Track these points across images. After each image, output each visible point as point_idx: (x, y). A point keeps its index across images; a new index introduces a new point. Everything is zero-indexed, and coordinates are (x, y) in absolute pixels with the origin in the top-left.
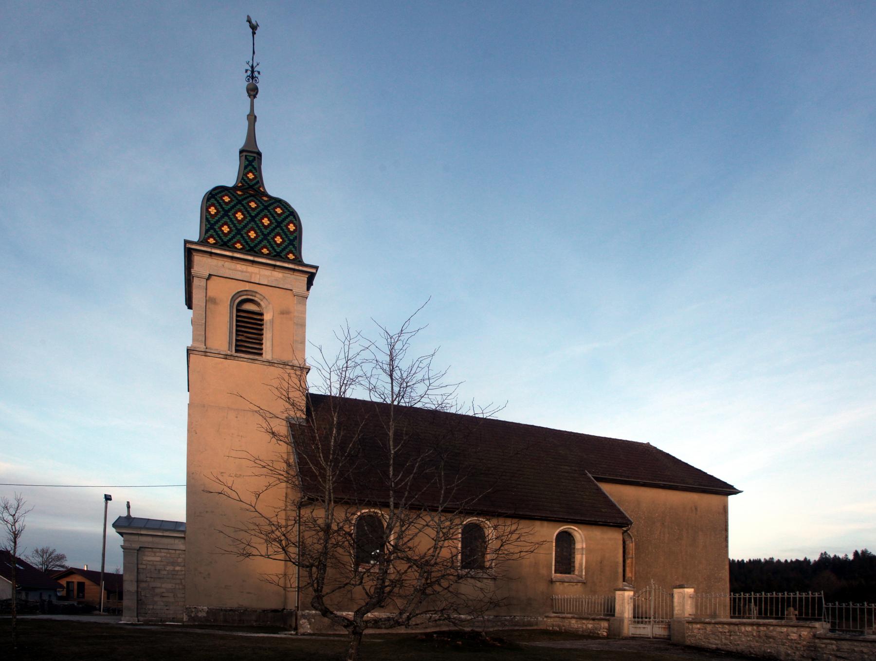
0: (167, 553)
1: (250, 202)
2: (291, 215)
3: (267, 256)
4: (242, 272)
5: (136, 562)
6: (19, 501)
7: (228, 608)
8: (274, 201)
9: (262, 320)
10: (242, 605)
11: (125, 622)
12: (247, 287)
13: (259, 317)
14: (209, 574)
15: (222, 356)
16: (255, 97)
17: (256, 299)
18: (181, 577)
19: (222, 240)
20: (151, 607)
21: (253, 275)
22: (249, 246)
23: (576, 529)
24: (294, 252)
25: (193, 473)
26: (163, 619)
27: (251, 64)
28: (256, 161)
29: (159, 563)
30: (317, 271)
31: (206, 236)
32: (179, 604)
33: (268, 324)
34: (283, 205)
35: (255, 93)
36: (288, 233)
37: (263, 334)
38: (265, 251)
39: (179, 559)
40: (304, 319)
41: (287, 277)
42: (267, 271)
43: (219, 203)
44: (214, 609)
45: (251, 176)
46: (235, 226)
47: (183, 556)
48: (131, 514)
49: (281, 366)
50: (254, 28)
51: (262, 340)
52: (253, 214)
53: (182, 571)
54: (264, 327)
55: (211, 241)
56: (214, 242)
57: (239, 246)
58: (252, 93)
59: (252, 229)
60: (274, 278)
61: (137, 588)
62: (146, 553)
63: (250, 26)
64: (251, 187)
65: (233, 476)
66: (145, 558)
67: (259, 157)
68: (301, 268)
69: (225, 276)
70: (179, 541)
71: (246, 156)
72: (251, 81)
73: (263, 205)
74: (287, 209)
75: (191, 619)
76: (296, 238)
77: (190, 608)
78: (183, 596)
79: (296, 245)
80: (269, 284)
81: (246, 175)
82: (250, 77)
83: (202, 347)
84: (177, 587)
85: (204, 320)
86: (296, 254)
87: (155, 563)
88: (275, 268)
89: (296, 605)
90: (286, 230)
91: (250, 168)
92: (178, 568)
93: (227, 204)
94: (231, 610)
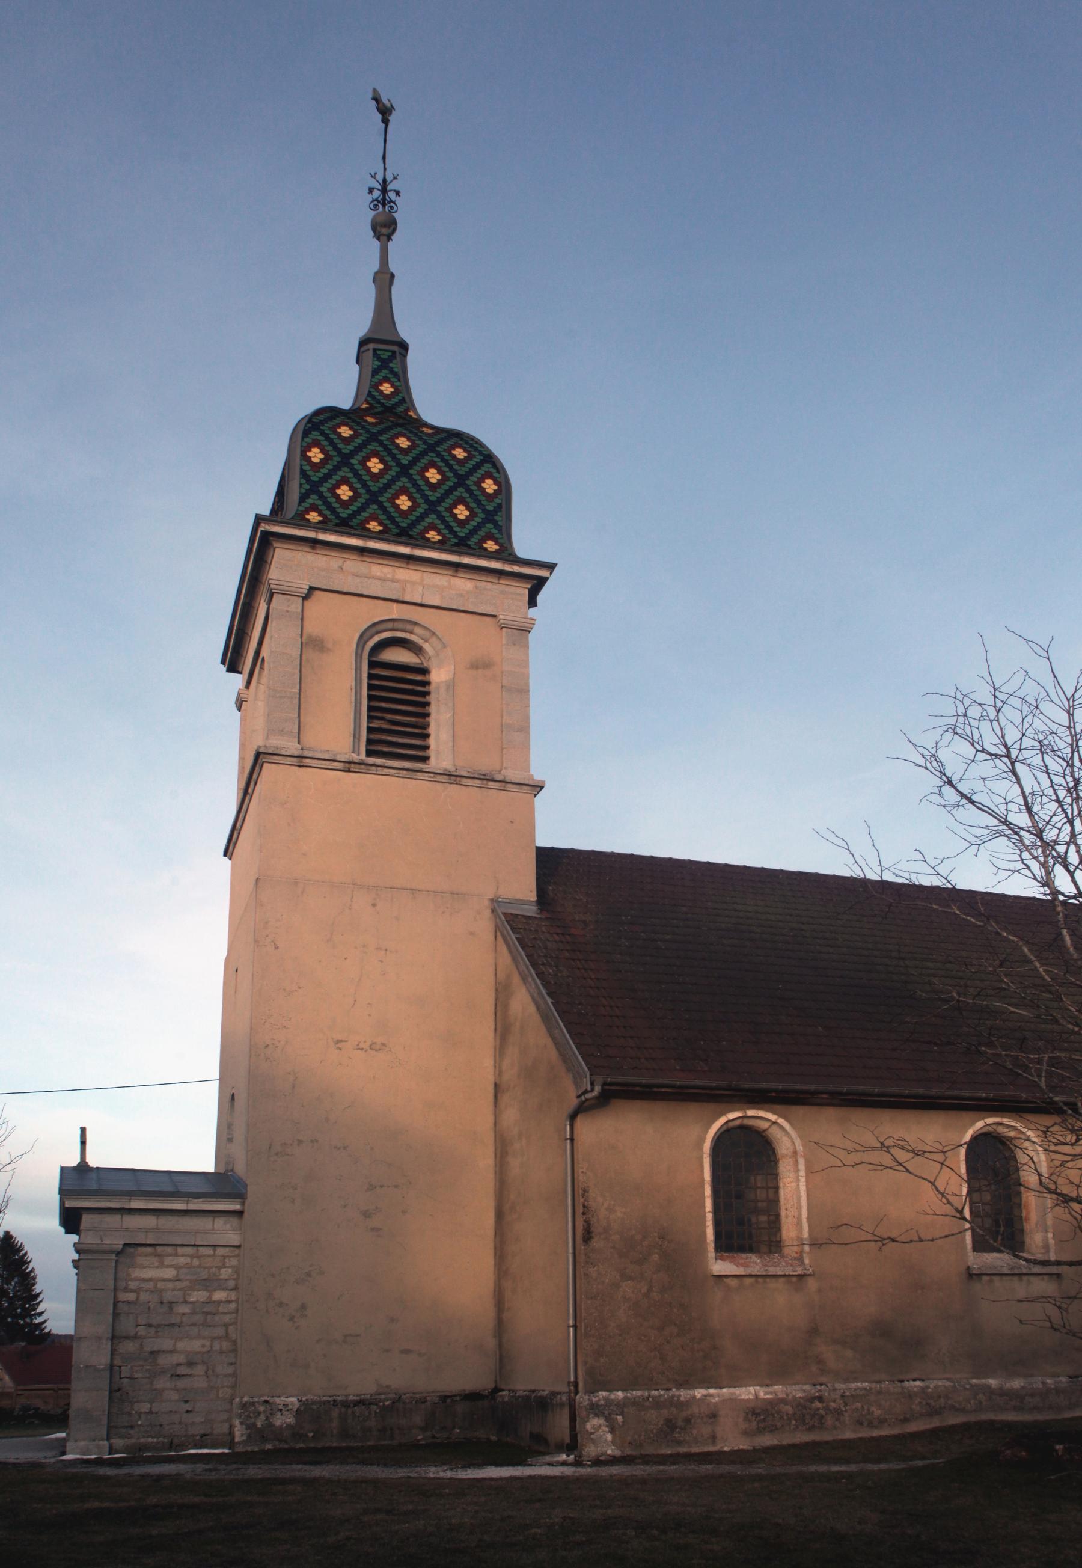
0: (192, 1257)
1: (397, 436)
2: (487, 462)
3: (440, 546)
4: (384, 580)
5: (112, 1287)
7: (351, 1398)
9: (427, 683)
10: (388, 1387)
11: (78, 1456)
12: (395, 612)
13: (419, 678)
14: (303, 1307)
15: (340, 766)
16: (389, 238)
17: (413, 638)
18: (227, 1319)
19: (338, 516)
20: (145, 1407)
21: (408, 585)
23: (773, 1117)
25: (267, 1046)
26: (176, 1441)
27: (380, 177)
29: (170, 1285)
31: (301, 508)
32: (221, 1396)
33: (442, 690)
34: (467, 443)
35: (390, 231)
36: (482, 498)
37: (428, 715)
38: (433, 535)
39: (223, 1271)
40: (527, 677)
41: (485, 589)
44: (314, 1403)
45: (387, 388)
46: (365, 485)
47: (234, 1262)
48: (87, 1160)
49: (478, 783)
50: (385, 112)
51: (426, 726)
52: (405, 461)
53: (230, 1302)
54: (432, 698)
55: (314, 517)
56: (321, 519)
57: (374, 526)
58: (384, 231)
59: (404, 491)
61: (112, 1359)
62: (140, 1260)
63: (378, 109)
64: (390, 410)
65: (366, 1046)
66: (137, 1273)
67: (403, 352)
68: (516, 569)
70: (225, 1223)
71: (375, 350)
72: (381, 209)
73: (425, 442)
74: (476, 449)
75: (256, 1434)
76: (499, 506)
77: (253, 1404)
78: (230, 1370)
79: (500, 523)
80: (444, 606)
81: (376, 386)
82: (379, 202)
83: (292, 747)
84: (217, 1346)
85: (298, 686)
86: (500, 541)
87: (160, 1285)
88: (456, 571)
89: (572, 1379)
90: (477, 493)
91: (384, 373)
92: (219, 1295)
93: (347, 441)
94: (357, 1403)
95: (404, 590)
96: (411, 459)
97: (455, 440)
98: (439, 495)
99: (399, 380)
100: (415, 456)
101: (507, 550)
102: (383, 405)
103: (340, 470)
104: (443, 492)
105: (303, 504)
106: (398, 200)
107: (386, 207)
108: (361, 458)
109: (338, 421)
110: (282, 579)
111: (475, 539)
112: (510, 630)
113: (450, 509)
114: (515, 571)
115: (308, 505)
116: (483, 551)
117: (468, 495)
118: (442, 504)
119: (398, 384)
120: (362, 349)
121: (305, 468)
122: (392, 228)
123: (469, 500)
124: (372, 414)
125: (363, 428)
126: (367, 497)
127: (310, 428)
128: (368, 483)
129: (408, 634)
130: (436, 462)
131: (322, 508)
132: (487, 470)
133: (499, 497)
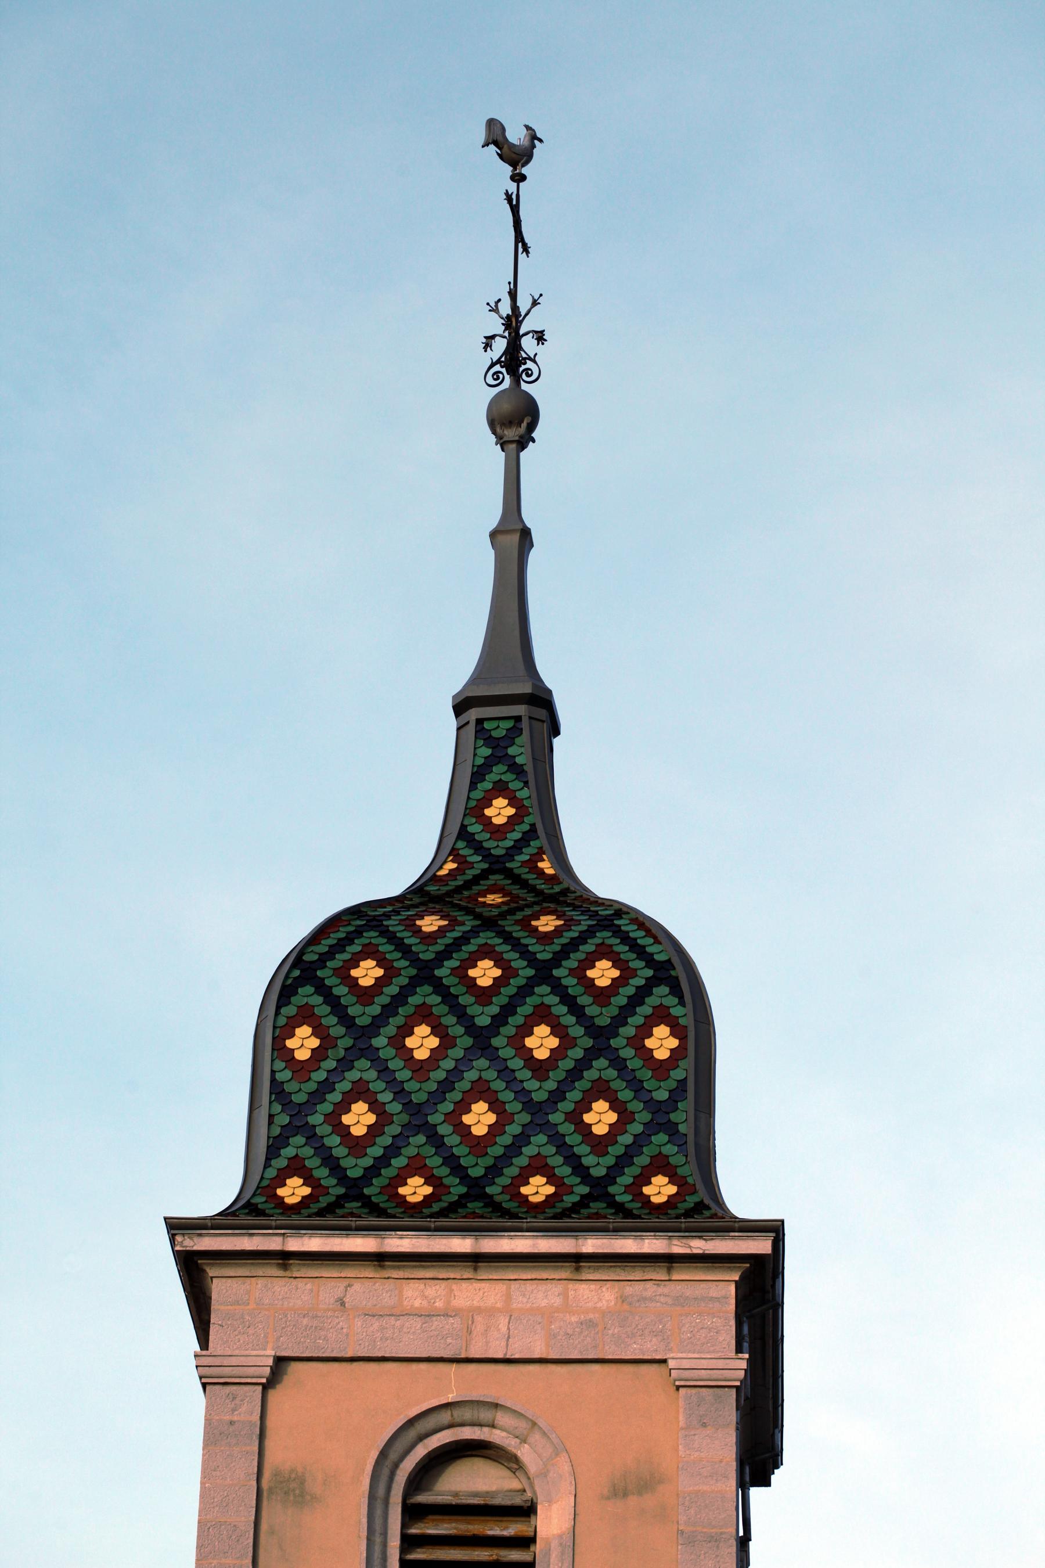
4: (427, 1315)
6: (486, 351)
13: (512, 1529)
16: (524, 442)
21: (478, 1319)
24: (677, 1160)
27: (505, 309)
28: (524, 739)
42: (543, 1287)
46: (400, 1093)
58: (511, 433)
60: (574, 1319)
63: (501, 156)
67: (542, 713)
81: (477, 810)
88: (578, 1269)
95: (470, 1332)
112: (694, 1391)
114: (695, 1251)
121: (279, 1077)
122: (524, 425)
127: (295, 978)
129: (486, 1429)
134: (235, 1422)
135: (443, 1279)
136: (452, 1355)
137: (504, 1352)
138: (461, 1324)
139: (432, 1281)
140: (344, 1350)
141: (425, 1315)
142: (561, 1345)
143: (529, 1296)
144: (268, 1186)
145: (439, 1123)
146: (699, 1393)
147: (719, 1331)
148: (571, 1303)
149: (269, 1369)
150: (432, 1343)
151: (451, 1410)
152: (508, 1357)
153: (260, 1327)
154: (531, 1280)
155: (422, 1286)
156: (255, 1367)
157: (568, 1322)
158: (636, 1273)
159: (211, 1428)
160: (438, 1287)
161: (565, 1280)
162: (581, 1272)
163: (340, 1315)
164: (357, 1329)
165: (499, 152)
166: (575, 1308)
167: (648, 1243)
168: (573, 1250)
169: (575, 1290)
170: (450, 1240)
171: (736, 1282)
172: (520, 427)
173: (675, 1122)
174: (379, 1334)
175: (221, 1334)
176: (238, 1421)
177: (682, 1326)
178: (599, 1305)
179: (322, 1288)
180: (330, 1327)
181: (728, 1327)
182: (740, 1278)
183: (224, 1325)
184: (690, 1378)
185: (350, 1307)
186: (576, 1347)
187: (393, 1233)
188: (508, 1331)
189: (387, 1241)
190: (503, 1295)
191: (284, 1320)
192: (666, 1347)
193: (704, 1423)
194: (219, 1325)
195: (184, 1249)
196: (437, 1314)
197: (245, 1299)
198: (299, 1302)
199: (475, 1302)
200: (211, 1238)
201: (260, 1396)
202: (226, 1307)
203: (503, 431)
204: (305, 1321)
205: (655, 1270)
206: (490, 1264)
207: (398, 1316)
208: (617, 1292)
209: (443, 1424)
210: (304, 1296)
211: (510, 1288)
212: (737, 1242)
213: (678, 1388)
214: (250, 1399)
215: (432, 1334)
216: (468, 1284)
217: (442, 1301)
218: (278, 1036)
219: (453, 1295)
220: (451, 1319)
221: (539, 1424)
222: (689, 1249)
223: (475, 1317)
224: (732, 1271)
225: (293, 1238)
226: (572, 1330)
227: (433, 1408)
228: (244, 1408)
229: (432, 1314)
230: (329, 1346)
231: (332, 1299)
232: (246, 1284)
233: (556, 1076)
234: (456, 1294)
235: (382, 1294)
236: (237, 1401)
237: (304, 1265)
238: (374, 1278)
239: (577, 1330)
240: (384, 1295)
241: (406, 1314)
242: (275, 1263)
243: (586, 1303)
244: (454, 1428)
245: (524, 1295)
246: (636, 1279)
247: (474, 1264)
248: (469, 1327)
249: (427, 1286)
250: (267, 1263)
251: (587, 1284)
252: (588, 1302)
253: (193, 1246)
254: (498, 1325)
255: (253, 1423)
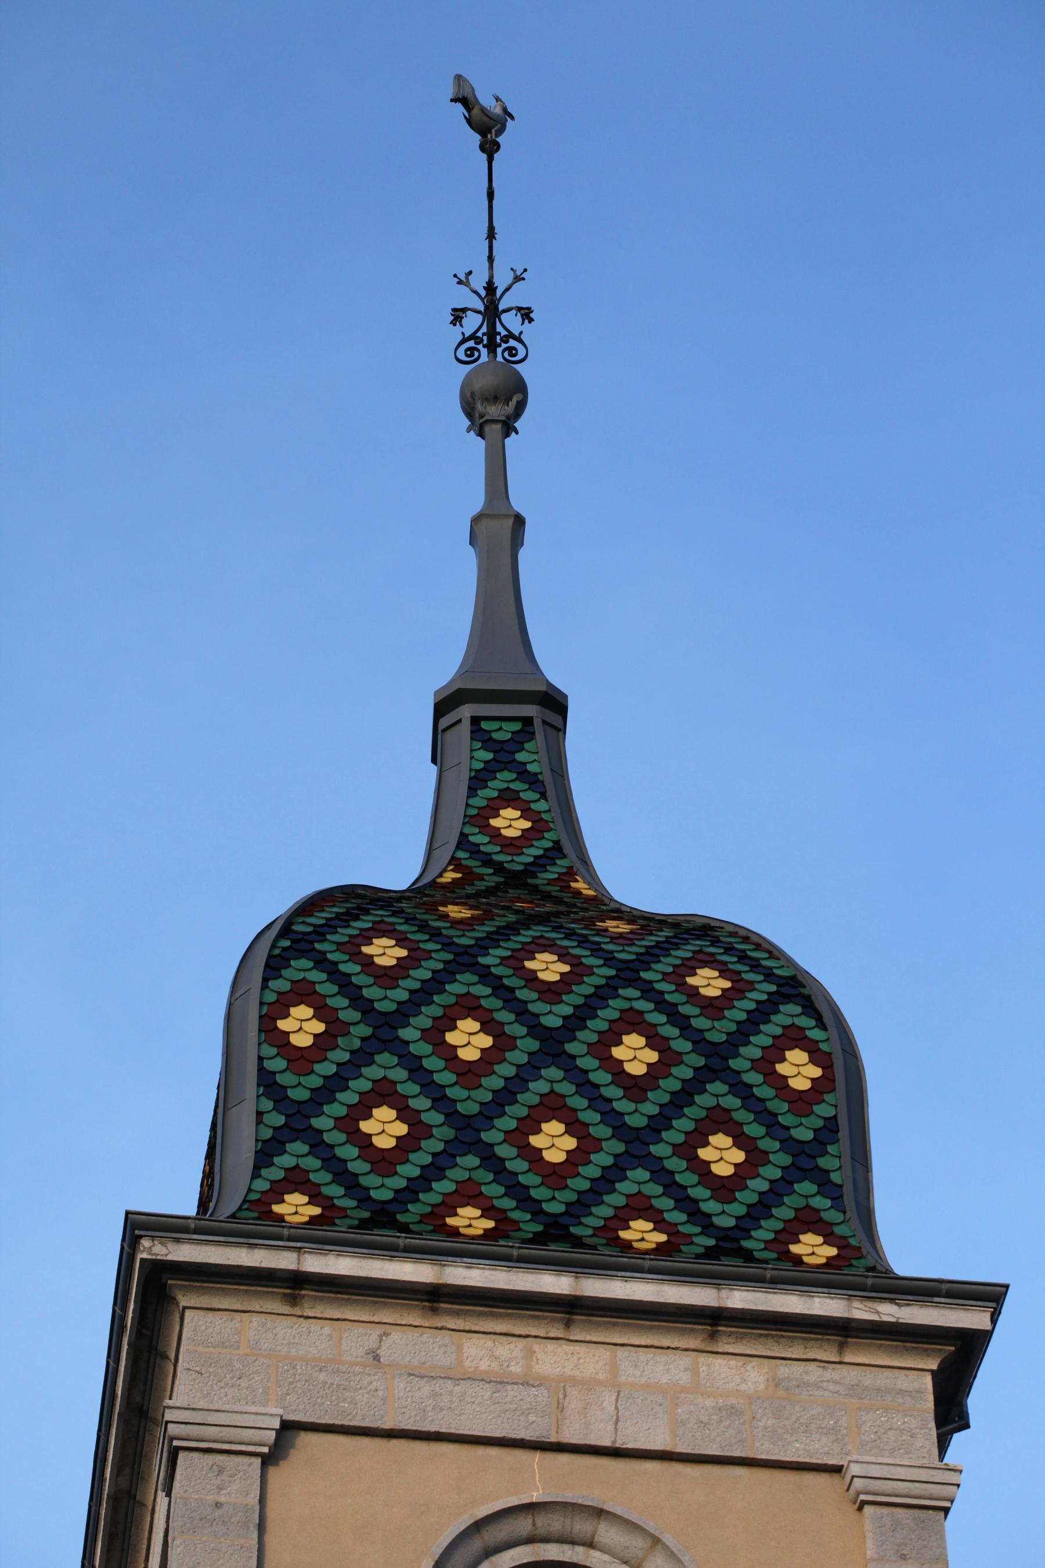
1: (689, 967)
2: (788, 999)
4: (500, 1382)
8: (667, 933)
16: (508, 428)
19: (364, 1198)
21: (572, 1392)
22: (537, 1212)
27: (479, 282)
30: (994, 1320)
31: (261, 1185)
34: (729, 950)
41: (803, 1385)
42: (662, 1357)
43: (345, 985)
46: (440, 1100)
58: (494, 411)
60: (709, 1403)
63: (469, 121)
67: (554, 719)
68: (888, 1312)
69: (388, 1424)
71: (475, 721)
73: (609, 960)
74: (755, 966)
76: (831, 1126)
79: (836, 1177)
80: (682, 1448)
81: (481, 819)
82: (479, 341)
86: (839, 1230)
88: (713, 1336)
90: (764, 1092)
91: (504, 779)
93: (387, 977)
96: (569, 1010)
97: (696, 944)
98: (655, 1110)
99: (544, 796)
100: (581, 1001)
101: (861, 1257)
102: (499, 868)
103: (371, 1063)
104: (666, 1098)
105: (264, 1172)
106: (528, 331)
107: (499, 350)
108: (428, 1023)
109: (364, 923)
110: (202, 1404)
111: (764, 1233)
112: (886, 1510)
113: (688, 1149)
114: (885, 1318)
115: (280, 1175)
116: (788, 1265)
117: (737, 1102)
118: (665, 1135)
119: (542, 806)
120: (444, 722)
121: (270, 1065)
122: (513, 403)
123: (741, 1116)
124: (469, 896)
125: (435, 935)
126: (449, 1133)
127: (284, 949)
128: (449, 1092)
129: (580, 1549)
130: (641, 1013)
131: (321, 1177)
132: (788, 1021)
133: (829, 1098)
134: (221, 1504)
135: (520, 1336)
136: (537, 1437)
137: (612, 1439)
138: (549, 1397)
139: (505, 1338)
140: (380, 1419)
141: (496, 1382)
142: (693, 1436)
143: (644, 1368)
144: (259, 1200)
145: (497, 1142)
146: (893, 1513)
147: (914, 1434)
148: (702, 1382)
149: (273, 1434)
150: (508, 1419)
151: (533, 1515)
152: (617, 1445)
153: (257, 1378)
154: (646, 1347)
155: (490, 1344)
156: (253, 1430)
157: (701, 1406)
158: (794, 1348)
159: (187, 1509)
160: (512, 1346)
161: (694, 1350)
162: (717, 1341)
163: (372, 1373)
164: (399, 1392)
165: (467, 114)
166: (709, 1389)
167: (820, 1302)
168: (714, 1303)
169: (708, 1365)
170: (539, 1276)
171: (932, 1371)
172: (508, 405)
173: (825, 1168)
174: (430, 1401)
175: (200, 1385)
176: (227, 1503)
177: (862, 1424)
178: (743, 1387)
179: (346, 1335)
180: (359, 1386)
181: (927, 1431)
182: (938, 1367)
183: (203, 1373)
184: (880, 1492)
185: (387, 1363)
186: (714, 1440)
187: (458, 1260)
188: (616, 1412)
189: (448, 1270)
190: (606, 1364)
191: (291, 1372)
192: (842, 1449)
193: (903, 1554)
194: (196, 1371)
195: (154, 1257)
196: (513, 1381)
197: (234, 1340)
198: (313, 1351)
199: (566, 1370)
200: (193, 1247)
201: (259, 1471)
202: (207, 1350)
203: (485, 409)
204: (322, 1377)
205: (821, 1346)
206: (590, 1318)
207: (458, 1380)
208: (767, 1373)
209: (521, 1536)
210: (321, 1343)
211: (616, 1356)
212: (942, 1311)
213: (864, 1503)
214: (245, 1474)
215: (506, 1407)
216: (556, 1346)
217: (520, 1364)
218: (266, 1014)
219: (534, 1358)
220: (534, 1389)
221: (665, 1540)
222: (877, 1315)
223: (568, 1390)
224: (928, 1355)
225: (313, 1256)
226: (707, 1418)
227: (510, 1508)
228: (235, 1487)
229: (505, 1380)
230: (359, 1412)
231: (361, 1350)
232: (234, 1321)
233: (658, 1097)
234: (539, 1358)
235: (433, 1348)
236: (224, 1477)
237: (321, 1299)
238: (421, 1326)
239: (714, 1417)
240: (436, 1350)
241: (469, 1378)
242: (279, 1293)
243: (725, 1383)
244: (533, 1544)
245: (636, 1366)
246: (794, 1356)
247: (567, 1316)
248: (560, 1401)
249: (497, 1343)
250: (268, 1293)
251: (724, 1359)
252: (728, 1383)
253: (166, 1255)
254: (602, 1403)
255: (249, 1507)
